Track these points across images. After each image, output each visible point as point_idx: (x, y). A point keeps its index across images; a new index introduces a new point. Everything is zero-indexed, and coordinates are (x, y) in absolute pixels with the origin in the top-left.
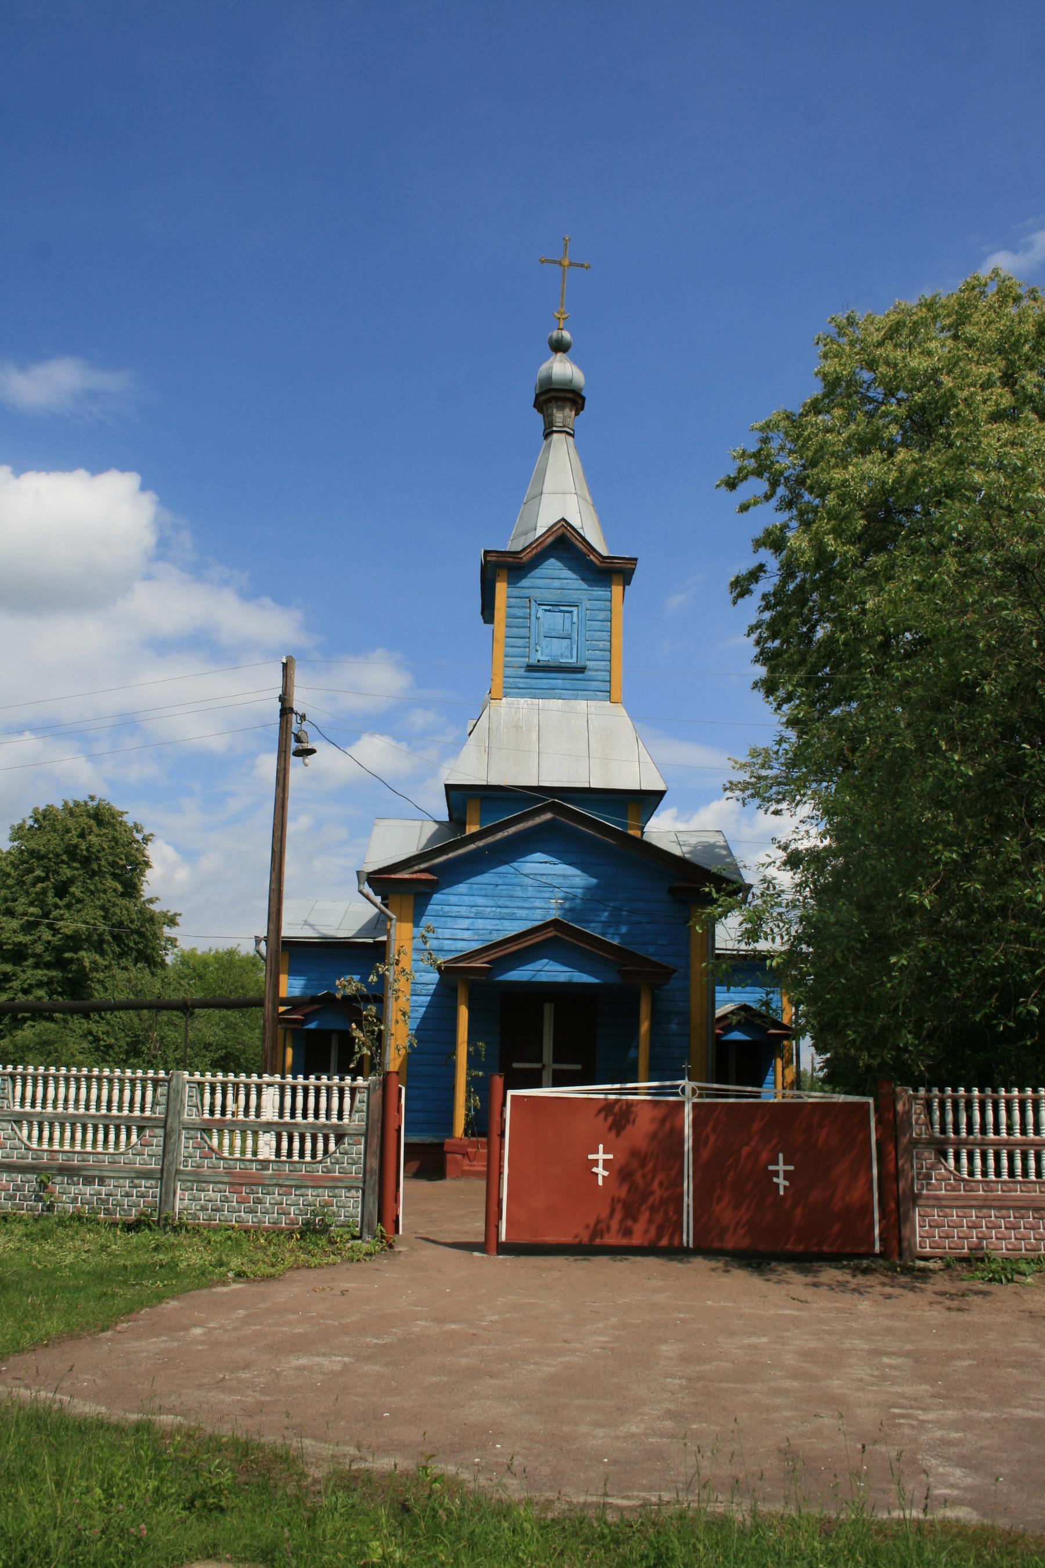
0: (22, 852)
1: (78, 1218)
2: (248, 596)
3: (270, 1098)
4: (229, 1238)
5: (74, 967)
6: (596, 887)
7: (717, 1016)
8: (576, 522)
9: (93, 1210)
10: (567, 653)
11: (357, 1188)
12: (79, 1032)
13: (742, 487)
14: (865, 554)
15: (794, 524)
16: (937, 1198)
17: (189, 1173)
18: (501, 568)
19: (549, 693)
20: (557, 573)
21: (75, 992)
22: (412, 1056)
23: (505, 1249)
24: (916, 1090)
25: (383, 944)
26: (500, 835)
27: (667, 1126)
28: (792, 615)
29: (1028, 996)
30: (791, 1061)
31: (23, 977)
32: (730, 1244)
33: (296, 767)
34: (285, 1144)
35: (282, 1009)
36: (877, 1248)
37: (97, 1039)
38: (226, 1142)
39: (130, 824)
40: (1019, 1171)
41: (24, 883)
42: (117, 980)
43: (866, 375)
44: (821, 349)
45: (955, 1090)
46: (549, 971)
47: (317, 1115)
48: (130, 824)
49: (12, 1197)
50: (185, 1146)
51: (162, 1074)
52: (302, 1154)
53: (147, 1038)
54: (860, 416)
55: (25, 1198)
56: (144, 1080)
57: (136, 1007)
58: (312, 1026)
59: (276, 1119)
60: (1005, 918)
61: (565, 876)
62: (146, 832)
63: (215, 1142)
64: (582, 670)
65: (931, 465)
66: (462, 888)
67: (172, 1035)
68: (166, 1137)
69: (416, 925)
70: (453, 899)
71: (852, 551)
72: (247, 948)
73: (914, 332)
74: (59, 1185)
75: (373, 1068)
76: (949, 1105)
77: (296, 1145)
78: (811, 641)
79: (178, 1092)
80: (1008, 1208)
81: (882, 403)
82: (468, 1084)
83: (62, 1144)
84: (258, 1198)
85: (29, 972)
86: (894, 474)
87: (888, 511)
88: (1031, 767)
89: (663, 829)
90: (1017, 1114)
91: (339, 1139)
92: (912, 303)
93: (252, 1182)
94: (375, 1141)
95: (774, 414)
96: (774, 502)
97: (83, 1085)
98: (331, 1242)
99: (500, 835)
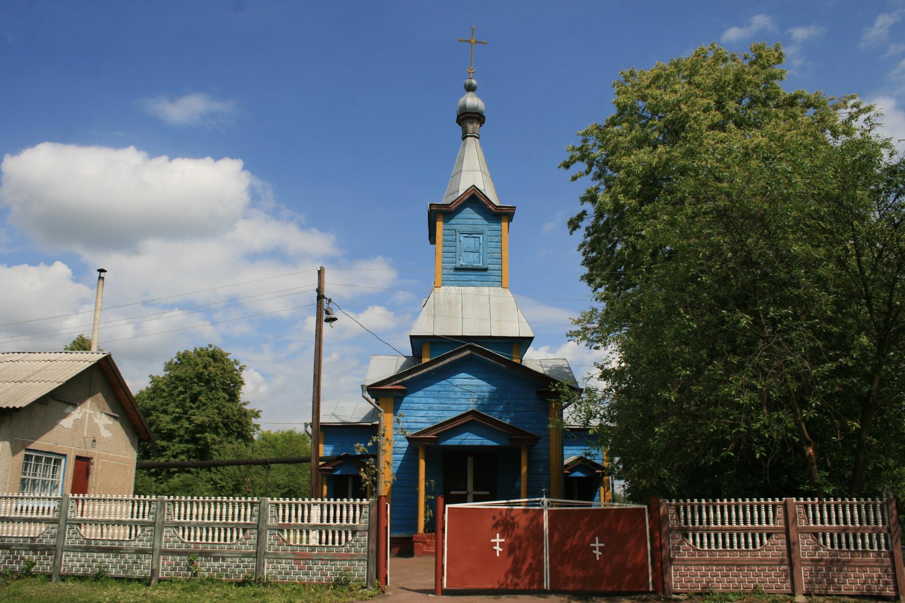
0: (171, 377)
1: (211, 579)
2: (303, 227)
3: (316, 511)
4: (294, 589)
5: (202, 442)
6: (496, 391)
7: (566, 462)
8: (481, 187)
9: (220, 576)
10: (477, 260)
11: (364, 560)
12: (205, 479)
13: (572, 167)
14: (642, 205)
15: (602, 187)
16: (684, 560)
17: (272, 554)
18: (440, 214)
19: (468, 283)
20: (471, 216)
21: (202, 457)
22: (394, 486)
23: (446, 592)
24: (670, 501)
25: (377, 426)
26: (441, 364)
27: (535, 522)
28: (603, 238)
29: (728, 447)
30: (609, 489)
31: (173, 448)
32: (571, 587)
33: (326, 326)
34: (324, 537)
35: (321, 463)
36: (651, 589)
37: (216, 483)
38: (292, 536)
39: (232, 360)
40: (728, 544)
41: (172, 395)
42: (226, 449)
43: (641, 104)
44: (616, 90)
45: (692, 501)
46: (470, 439)
47: (341, 521)
48: (232, 360)
49: (174, 569)
50: (269, 539)
51: (256, 499)
52: (333, 543)
53: (244, 482)
54: (637, 126)
55: (182, 569)
56: (239, 503)
57: (237, 463)
58: (338, 473)
59: (319, 523)
60: (716, 407)
61: (478, 386)
62: (242, 364)
63: (286, 536)
64: (486, 270)
65: (676, 154)
66: (420, 393)
67: (258, 480)
68: (259, 534)
69: (395, 415)
70: (415, 400)
71: (634, 202)
72: (300, 429)
73: (667, 79)
74: (200, 562)
75: (372, 494)
76: (689, 509)
77: (330, 537)
78: (613, 253)
79: (265, 509)
80: (723, 565)
81: (651, 119)
82: (426, 503)
83: (199, 539)
85: (177, 445)
86: (656, 160)
87: (655, 179)
88: (727, 322)
89: (535, 359)
90: (726, 513)
91: (354, 533)
92: (665, 64)
93: (306, 558)
94: (374, 534)
95: (589, 126)
96: (591, 175)
97: (213, 506)
98: (351, 590)
99: (441, 364)
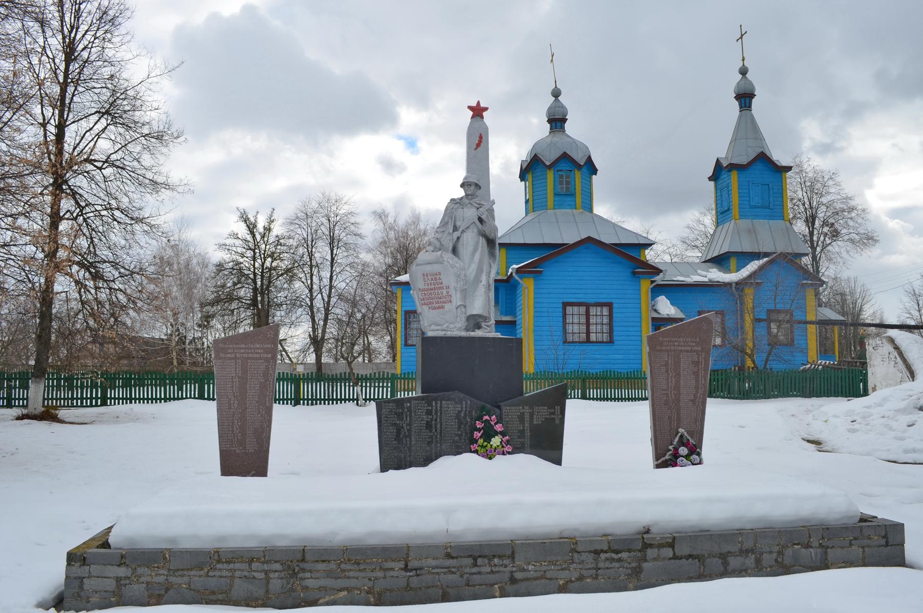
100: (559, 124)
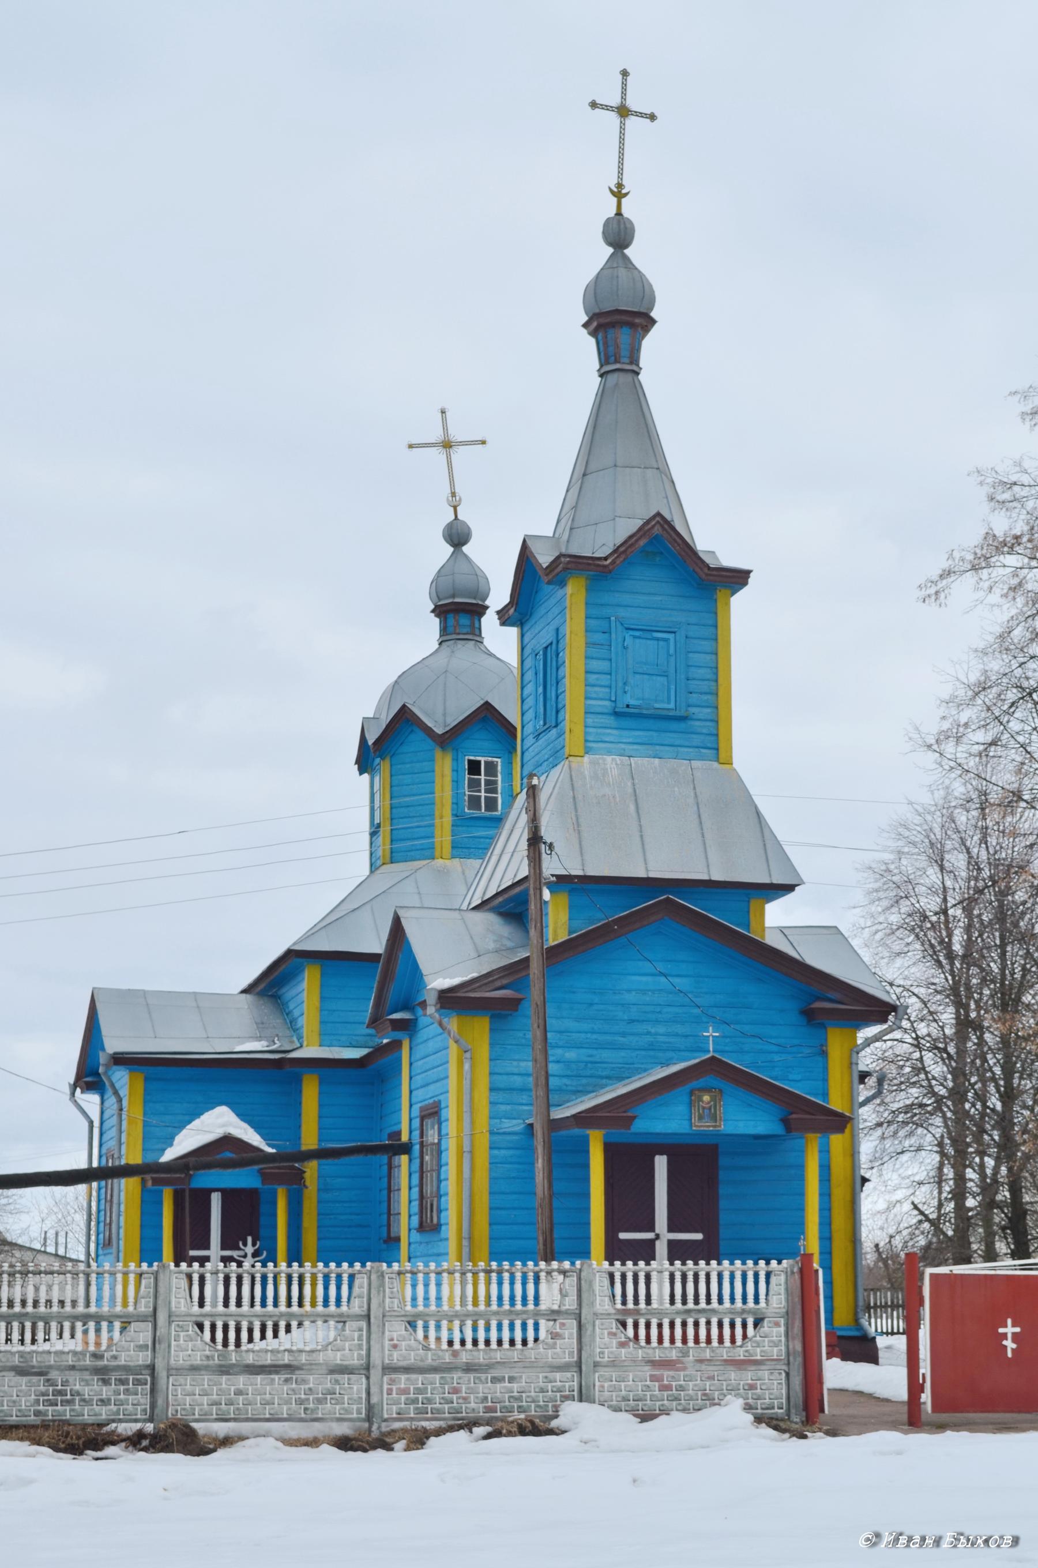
68: (580, 1326)
84: (681, 1386)
100: (464, 620)
